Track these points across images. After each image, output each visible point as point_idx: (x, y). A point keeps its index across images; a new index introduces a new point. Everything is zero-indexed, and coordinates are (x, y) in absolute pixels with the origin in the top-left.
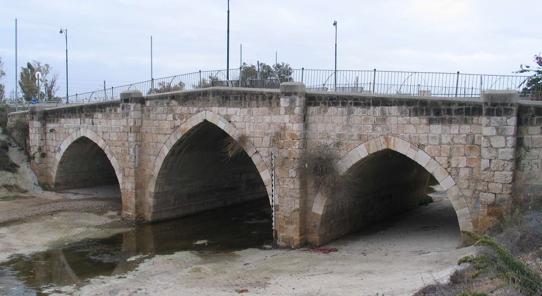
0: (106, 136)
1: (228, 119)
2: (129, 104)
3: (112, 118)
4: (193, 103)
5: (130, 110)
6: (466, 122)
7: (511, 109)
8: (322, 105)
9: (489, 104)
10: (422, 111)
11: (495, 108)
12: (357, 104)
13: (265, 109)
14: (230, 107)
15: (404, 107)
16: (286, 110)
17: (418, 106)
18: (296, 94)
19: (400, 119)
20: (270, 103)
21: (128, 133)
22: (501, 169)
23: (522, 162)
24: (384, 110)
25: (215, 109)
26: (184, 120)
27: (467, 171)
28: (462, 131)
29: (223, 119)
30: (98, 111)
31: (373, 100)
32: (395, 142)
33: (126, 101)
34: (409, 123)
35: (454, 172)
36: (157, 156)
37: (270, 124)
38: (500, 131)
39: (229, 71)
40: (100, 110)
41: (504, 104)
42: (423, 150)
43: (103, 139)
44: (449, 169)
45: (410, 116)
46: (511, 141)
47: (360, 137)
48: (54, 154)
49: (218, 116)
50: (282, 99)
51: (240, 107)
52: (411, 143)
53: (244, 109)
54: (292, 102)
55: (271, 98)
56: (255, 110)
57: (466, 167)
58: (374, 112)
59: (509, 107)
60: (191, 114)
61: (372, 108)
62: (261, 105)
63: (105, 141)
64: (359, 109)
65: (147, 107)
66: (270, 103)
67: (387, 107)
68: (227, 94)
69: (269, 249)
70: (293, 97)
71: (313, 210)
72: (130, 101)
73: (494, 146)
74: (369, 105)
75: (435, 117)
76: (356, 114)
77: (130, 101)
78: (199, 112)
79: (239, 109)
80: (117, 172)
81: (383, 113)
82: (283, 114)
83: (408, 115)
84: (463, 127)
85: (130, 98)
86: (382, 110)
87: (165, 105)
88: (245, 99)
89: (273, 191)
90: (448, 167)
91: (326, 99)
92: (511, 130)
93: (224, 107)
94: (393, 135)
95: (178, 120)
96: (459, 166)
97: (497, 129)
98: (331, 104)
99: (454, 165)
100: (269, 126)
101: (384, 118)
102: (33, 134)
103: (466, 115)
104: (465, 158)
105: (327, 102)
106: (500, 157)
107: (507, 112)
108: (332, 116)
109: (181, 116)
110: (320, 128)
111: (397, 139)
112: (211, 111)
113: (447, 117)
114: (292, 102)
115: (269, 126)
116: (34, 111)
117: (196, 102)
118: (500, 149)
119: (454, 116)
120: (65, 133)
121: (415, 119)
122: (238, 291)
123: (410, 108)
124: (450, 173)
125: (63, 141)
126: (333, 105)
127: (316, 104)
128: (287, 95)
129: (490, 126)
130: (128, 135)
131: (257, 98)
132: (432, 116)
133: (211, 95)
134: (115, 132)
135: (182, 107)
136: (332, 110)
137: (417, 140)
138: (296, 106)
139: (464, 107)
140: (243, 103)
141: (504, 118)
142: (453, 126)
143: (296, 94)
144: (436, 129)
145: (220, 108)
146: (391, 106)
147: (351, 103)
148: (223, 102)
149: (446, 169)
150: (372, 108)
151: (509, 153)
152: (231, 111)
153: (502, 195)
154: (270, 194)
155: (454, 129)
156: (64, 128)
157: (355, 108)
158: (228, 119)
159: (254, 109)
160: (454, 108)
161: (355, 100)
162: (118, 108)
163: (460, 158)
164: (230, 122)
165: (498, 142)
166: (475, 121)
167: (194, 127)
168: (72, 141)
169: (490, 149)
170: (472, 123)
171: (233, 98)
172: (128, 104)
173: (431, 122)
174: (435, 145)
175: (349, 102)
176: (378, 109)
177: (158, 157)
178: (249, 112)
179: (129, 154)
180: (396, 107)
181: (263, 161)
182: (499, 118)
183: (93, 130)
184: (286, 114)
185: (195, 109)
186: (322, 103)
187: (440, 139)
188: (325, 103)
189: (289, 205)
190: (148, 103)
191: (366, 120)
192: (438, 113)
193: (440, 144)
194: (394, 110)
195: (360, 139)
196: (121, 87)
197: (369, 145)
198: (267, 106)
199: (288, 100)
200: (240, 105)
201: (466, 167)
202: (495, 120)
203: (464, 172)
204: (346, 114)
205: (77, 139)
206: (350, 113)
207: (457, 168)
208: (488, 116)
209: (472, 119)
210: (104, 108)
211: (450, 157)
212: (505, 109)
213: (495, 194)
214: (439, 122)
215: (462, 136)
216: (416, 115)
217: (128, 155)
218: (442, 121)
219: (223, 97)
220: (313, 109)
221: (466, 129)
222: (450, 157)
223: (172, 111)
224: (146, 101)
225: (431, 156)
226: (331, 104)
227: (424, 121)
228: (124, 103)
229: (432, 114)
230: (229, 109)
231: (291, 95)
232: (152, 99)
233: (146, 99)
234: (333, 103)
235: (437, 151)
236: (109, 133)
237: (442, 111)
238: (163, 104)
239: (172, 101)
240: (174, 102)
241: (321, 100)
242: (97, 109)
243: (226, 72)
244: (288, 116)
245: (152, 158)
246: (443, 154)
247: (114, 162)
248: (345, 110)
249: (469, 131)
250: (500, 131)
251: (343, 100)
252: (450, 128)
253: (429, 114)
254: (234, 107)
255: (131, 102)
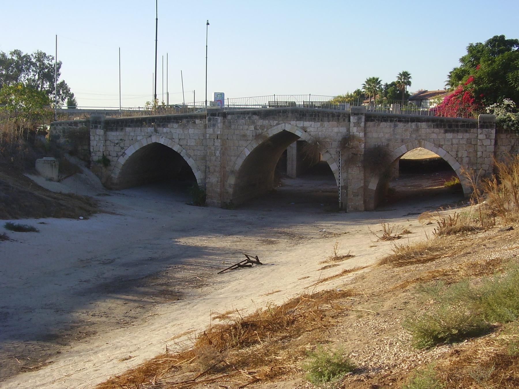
0: (183, 142)
1: (304, 129)
2: (217, 117)
3: (189, 127)
4: (274, 118)
5: (217, 122)
6: (466, 132)
7: (494, 125)
8: (377, 121)
9: (482, 122)
10: (441, 125)
11: (485, 124)
12: (400, 121)
13: (335, 123)
14: (306, 121)
15: (430, 123)
16: (354, 124)
17: (438, 123)
18: (362, 114)
19: (428, 130)
20: (338, 119)
21: (214, 139)
22: (488, 157)
23: (497, 153)
24: (418, 124)
25: (293, 123)
26: (266, 130)
27: (467, 159)
28: (464, 137)
29: (300, 130)
30: (174, 122)
31: (411, 119)
32: (425, 144)
33: (213, 115)
34: (433, 132)
35: (460, 160)
36: (238, 157)
37: (337, 133)
38: (488, 137)
39: (195, 103)
40: (175, 121)
41: (490, 122)
42: (442, 148)
43: (179, 144)
44: (457, 159)
45: (434, 128)
46: (493, 142)
47: (402, 141)
48: (117, 158)
49: (296, 128)
50: (351, 117)
51: (314, 121)
52: (435, 144)
53: (318, 123)
54: (360, 119)
55: (339, 116)
56: (326, 124)
57: (467, 157)
58: (411, 126)
59: (492, 124)
60: (271, 125)
61: (410, 123)
62: (331, 120)
63: (181, 146)
64: (401, 124)
65: (228, 120)
66: (338, 119)
67: (419, 123)
68: (303, 112)
69: (344, 213)
70: (360, 116)
71: (369, 188)
72: (217, 115)
73: (485, 145)
74: (408, 121)
75: (448, 129)
76: (399, 127)
77: (217, 115)
78: (279, 124)
79: (313, 122)
80: (194, 171)
81: (417, 126)
82: (353, 126)
83: (432, 128)
84: (465, 134)
85: (217, 113)
86: (416, 124)
87: (247, 118)
88: (319, 116)
89: (339, 177)
90: (457, 157)
91: (379, 117)
92: (493, 136)
93: (300, 121)
94: (423, 139)
95: (259, 129)
96: (463, 156)
97: (486, 135)
98: (383, 121)
99: (460, 156)
100: (337, 134)
101: (417, 130)
102: (96, 141)
103: (467, 128)
104: (466, 152)
105: (380, 119)
106: (488, 150)
107: (491, 127)
108: (383, 128)
109: (262, 127)
110: (375, 135)
111: (426, 142)
112: (290, 124)
113: (456, 129)
114: (360, 119)
115: (337, 134)
116: (98, 121)
117: (276, 117)
118: (488, 146)
119: (459, 128)
120: (132, 140)
121: (437, 130)
122: (211, 284)
123: (434, 123)
124: (457, 161)
125: (128, 147)
126: (384, 122)
127: (372, 121)
128: (355, 114)
129: (482, 134)
130: (214, 141)
131: (328, 115)
132: (447, 128)
133: (290, 113)
134: (193, 139)
135: (263, 120)
136: (383, 124)
137: (438, 142)
138: (362, 122)
139: (466, 123)
140: (317, 119)
141: (490, 130)
142: (459, 134)
143: (362, 114)
144: (449, 136)
145: (297, 122)
146: (422, 122)
147: (396, 120)
148: (301, 118)
149: (455, 158)
150: (410, 123)
151: (492, 148)
152: (307, 124)
153: (83, 322)
154: (337, 179)
155: (460, 136)
156: (132, 136)
157: (399, 123)
158: (304, 129)
159: (325, 123)
160: (460, 124)
161: (399, 118)
162: (197, 120)
163: (463, 152)
164: (306, 131)
165: (487, 142)
166: (471, 131)
167: (127, 160)
168: (141, 147)
169: (482, 146)
170: (470, 132)
171: (309, 115)
172: (215, 117)
173: (446, 132)
174: (449, 145)
175: (395, 119)
176: (414, 124)
177: (239, 158)
178: (321, 125)
179: (215, 155)
180: (425, 123)
181: (332, 157)
182: (487, 129)
183: (168, 137)
184: (354, 126)
185: (275, 122)
186: (376, 120)
187: (452, 141)
188: (378, 120)
189: (356, 184)
190: (229, 117)
191: (406, 130)
192: (450, 126)
193: (452, 144)
194: (424, 125)
195: (402, 142)
196: (282, 96)
197: (408, 146)
198: (336, 121)
199: (356, 118)
200: (314, 120)
201: (467, 157)
202: (485, 130)
203: (465, 160)
204: (318, 143)
205: (147, 144)
206: (395, 126)
207: (461, 158)
208: (481, 129)
209: (470, 130)
210: (181, 120)
211: (457, 151)
212: (490, 125)
213: (485, 170)
214: (451, 132)
215: (465, 139)
216: (437, 128)
217: (214, 156)
218: (453, 131)
219: (300, 115)
220: (370, 124)
221: (467, 136)
222: (457, 151)
223: (253, 123)
224: (227, 115)
225: (446, 151)
226: (383, 121)
227: (442, 131)
228: (211, 116)
229: (447, 127)
230: (305, 123)
231: (358, 115)
232: (233, 114)
233: (227, 114)
234: (384, 120)
235: (450, 148)
236: (186, 140)
237: (453, 126)
238: (245, 118)
239: (254, 116)
240: (256, 117)
241: (376, 118)
242: (173, 120)
243: (195, 102)
244: (356, 128)
245: (233, 158)
246: (453, 150)
247: (190, 162)
248: (392, 124)
249: (468, 136)
250: (487, 137)
251: (391, 118)
252: (458, 135)
253: (445, 127)
254: (309, 121)
255: (218, 116)
